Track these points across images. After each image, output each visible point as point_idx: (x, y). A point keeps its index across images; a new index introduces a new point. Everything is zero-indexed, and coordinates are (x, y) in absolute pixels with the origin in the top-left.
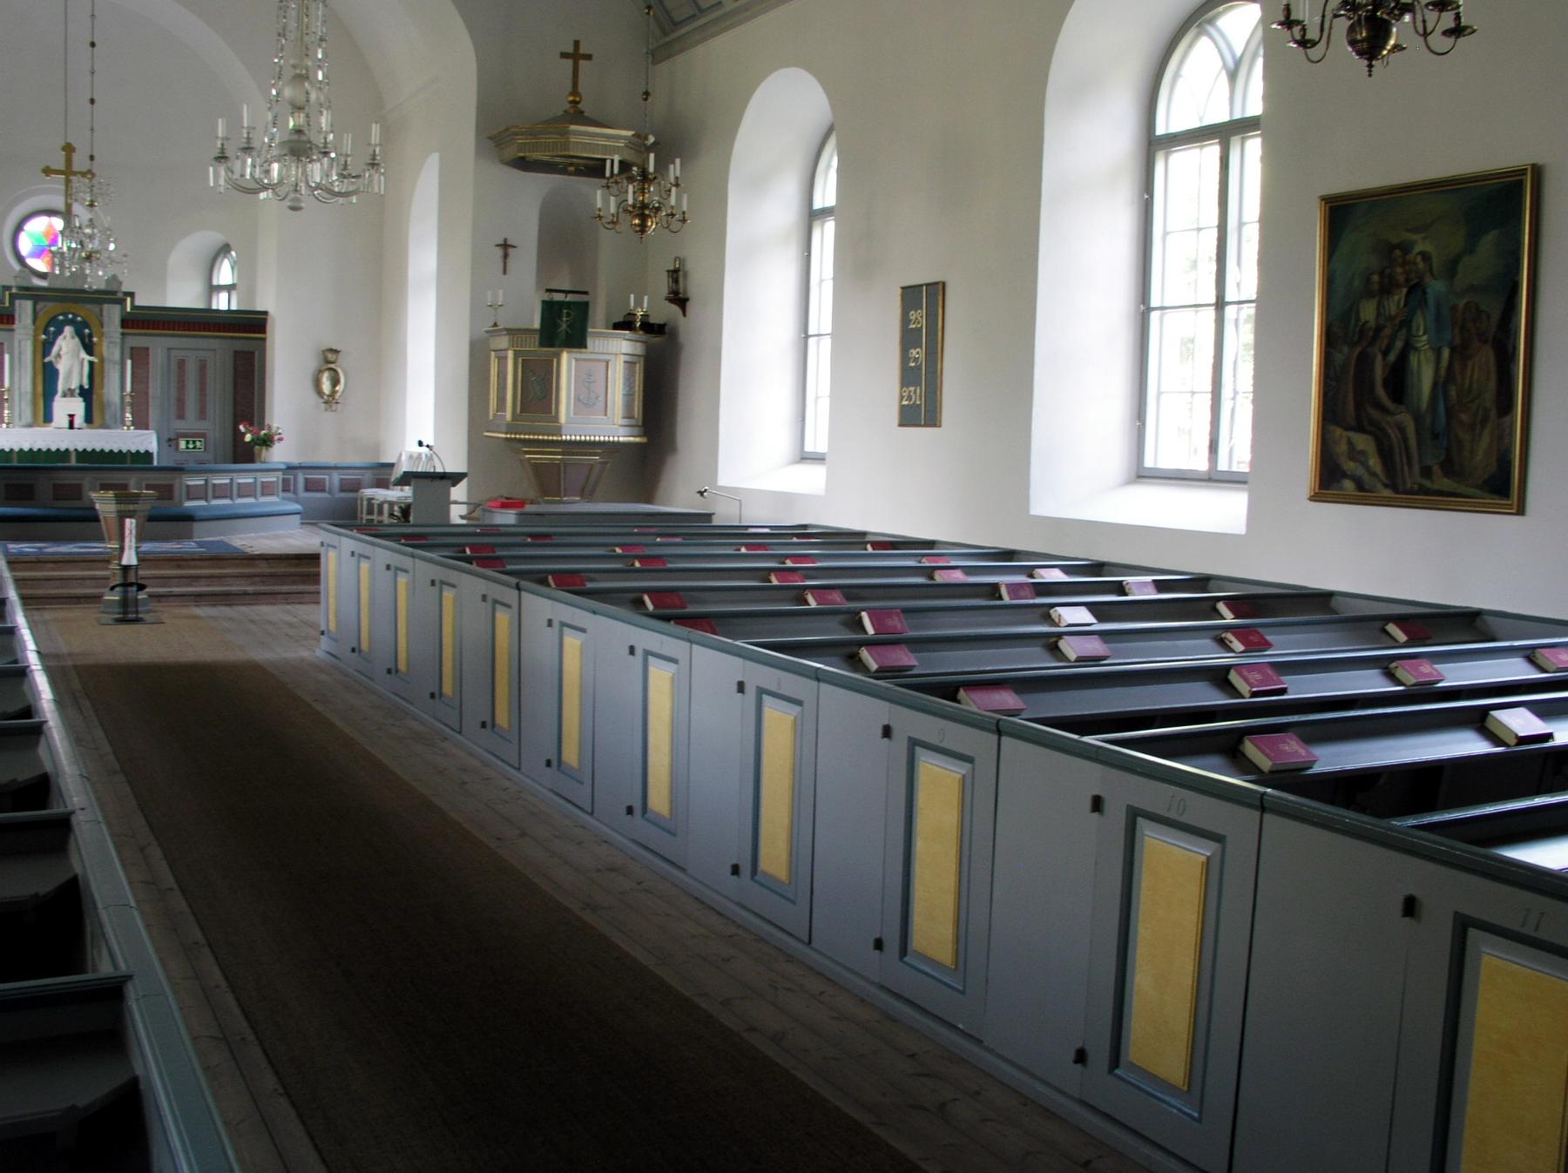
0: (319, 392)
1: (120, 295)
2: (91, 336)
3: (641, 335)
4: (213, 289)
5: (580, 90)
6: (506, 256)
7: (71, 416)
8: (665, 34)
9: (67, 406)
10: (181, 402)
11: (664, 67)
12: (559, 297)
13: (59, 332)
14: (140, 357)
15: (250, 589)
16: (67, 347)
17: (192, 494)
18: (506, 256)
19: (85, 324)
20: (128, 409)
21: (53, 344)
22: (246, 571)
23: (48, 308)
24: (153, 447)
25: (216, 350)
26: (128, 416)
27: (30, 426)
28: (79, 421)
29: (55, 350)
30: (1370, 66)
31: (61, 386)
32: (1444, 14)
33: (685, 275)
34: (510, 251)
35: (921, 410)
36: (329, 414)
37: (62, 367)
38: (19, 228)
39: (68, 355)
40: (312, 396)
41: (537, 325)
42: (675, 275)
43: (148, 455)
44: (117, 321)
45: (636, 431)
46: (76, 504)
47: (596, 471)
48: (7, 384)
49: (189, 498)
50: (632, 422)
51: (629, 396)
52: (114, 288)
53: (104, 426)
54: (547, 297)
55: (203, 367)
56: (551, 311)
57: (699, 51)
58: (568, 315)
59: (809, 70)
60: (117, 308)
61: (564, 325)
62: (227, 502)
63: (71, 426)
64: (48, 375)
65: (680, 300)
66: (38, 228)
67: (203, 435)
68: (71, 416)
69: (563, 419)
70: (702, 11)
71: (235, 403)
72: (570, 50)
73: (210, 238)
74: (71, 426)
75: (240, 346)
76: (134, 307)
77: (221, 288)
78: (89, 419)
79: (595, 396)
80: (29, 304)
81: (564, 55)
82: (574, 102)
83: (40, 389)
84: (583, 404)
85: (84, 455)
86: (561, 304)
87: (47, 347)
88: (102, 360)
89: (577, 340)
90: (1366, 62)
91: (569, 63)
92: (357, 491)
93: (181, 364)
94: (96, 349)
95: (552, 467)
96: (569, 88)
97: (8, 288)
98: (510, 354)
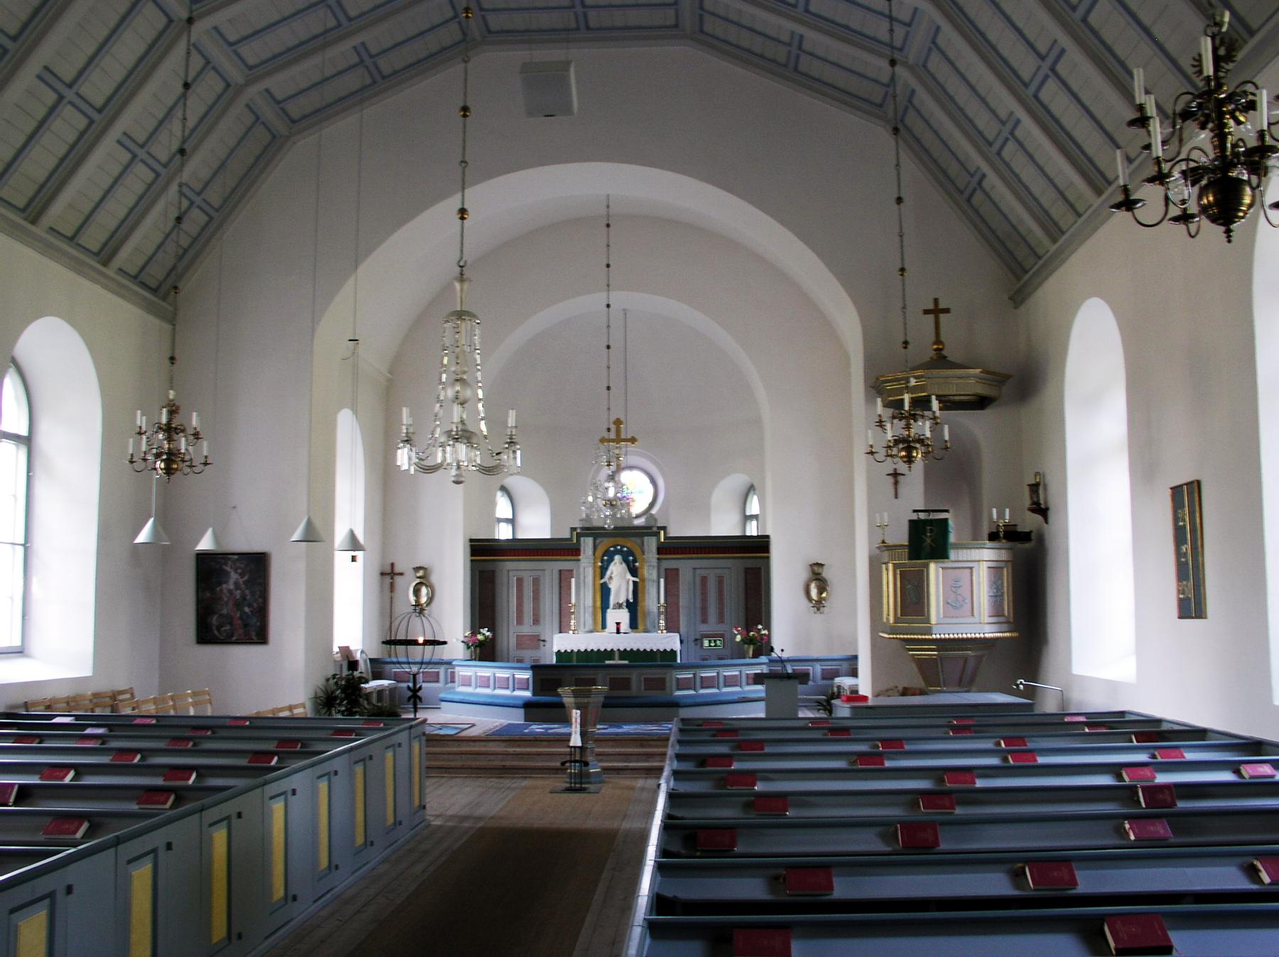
1: (655, 529)
3: (1004, 543)
4: (747, 518)
5: (943, 338)
6: (896, 483)
7: (618, 624)
10: (704, 611)
11: (1022, 309)
12: (922, 516)
13: (611, 560)
14: (671, 577)
16: (617, 569)
17: (682, 685)
18: (896, 483)
19: (630, 553)
20: (662, 617)
21: (607, 569)
23: (605, 543)
24: (677, 646)
25: (730, 568)
26: (662, 622)
27: (591, 632)
28: (625, 627)
29: (608, 573)
30: (1228, 232)
31: (612, 600)
33: (1045, 489)
35: (1192, 607)
36: (818, 616)
37: (613, 586)
38: (653, 482)
39: (619, 579)
42: (1034, 488)
43: (673, 652)
44: (654, 549)
47: (971, 664)
48: (573, 601)
49: (678, 689)
50: (1002, 619)
51: (997, 598)
52: (652, 523)
53: (646, 631)
54: (914, 516)
55: (720, 581)
56: (916, 527)
57: (1040, 293)
58: (931, 531)
59: (1107, 302)
60: (654, 539)
61: (927, 540)
62: (737, 689)
63: (618, 632)
64: (605, 591)
65: (1041, 510)
67: (722, 636)
68: (618, 624)
69: (933, 620)
71: (747, 609)
72: (931, 306)
73: (736, 481)
74: (618, 632)
75: (750, 564)
76: (666, 538)
78: (634, 625)
79: (966, 596)
80: (590, 541)
81: (926, 312)
83: (599, 604)
84: (952, 605)
85: (624, 654)
87: (603, 570)
88: (643, 580)
89: (940, 551)
90: (1223, 229)
91: (931, 317)
92: (832, 679)
93: (704, 580)
94: (640, 571)
95: (954, 660)
96: (933, 339)
98: (890, 566)
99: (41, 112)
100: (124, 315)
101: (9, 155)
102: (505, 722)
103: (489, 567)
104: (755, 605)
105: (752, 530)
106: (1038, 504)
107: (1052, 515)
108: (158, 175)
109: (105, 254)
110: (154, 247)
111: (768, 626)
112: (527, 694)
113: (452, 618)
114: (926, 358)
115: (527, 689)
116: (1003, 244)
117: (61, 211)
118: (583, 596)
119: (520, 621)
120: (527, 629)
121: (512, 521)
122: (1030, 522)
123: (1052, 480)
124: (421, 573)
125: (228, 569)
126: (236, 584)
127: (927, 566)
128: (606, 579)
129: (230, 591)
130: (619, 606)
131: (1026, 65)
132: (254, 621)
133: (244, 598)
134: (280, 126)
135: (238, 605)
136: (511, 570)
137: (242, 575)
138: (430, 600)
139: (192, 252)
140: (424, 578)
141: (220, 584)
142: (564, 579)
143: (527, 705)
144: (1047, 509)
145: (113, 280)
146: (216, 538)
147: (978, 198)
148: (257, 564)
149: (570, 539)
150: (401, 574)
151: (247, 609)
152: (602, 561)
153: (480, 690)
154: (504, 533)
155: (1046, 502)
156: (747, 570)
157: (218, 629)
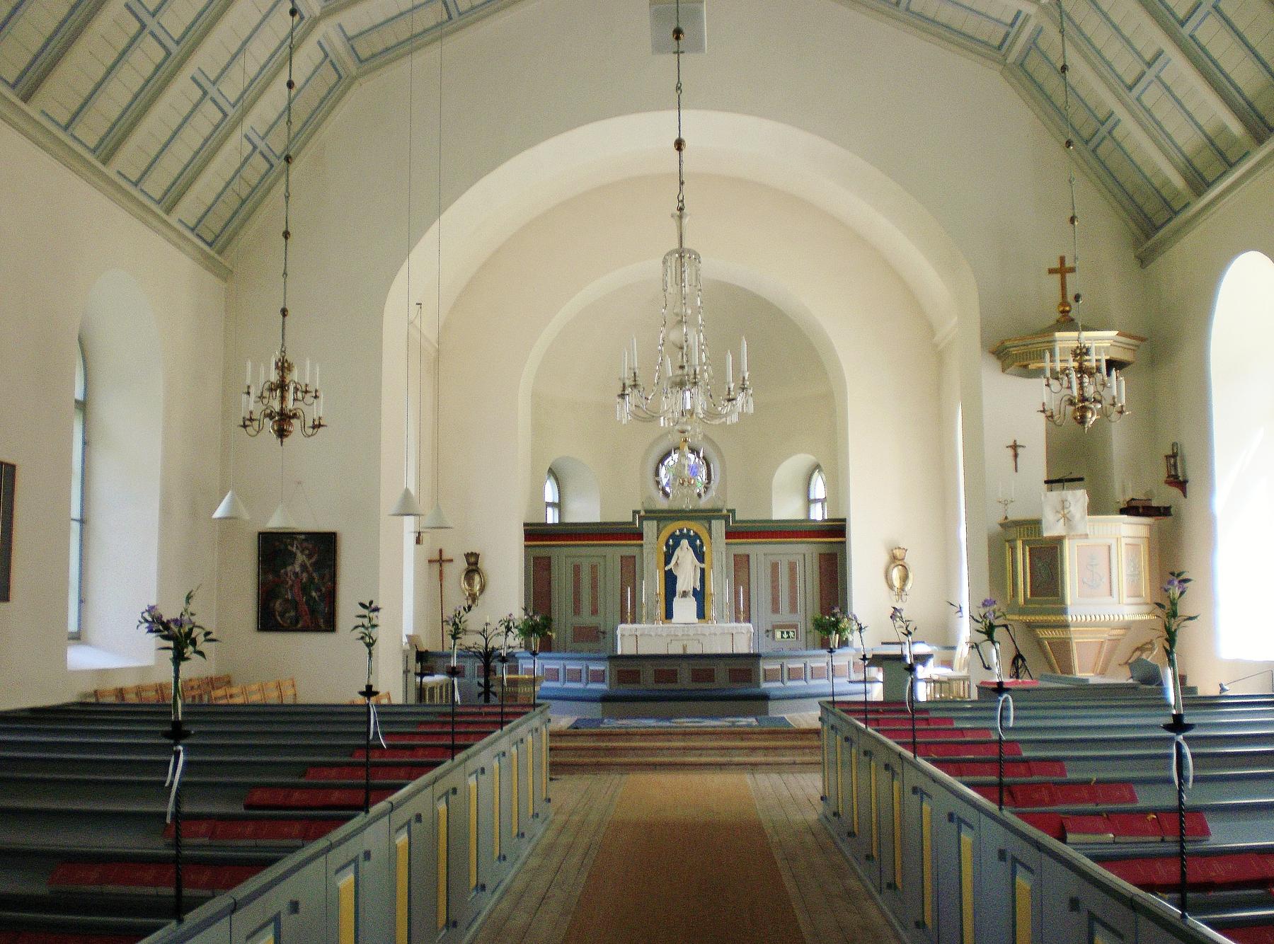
0: (891, 587)
1: (725, 512)
2: (702, 545)
6: (1016, 456)
8: (1148, 237)
9: (685, 609)
13: (677, 544)
15: (798, 759)
16: (685, 557)
17: (770, 676)
18: (1016, 456)
19: (697, 536)
22: (799, 743)
31: (680, 587)
32: (1199, 139)
33: (1183, 460)
34: (1020, 451)
45: (1144, 608)
46: (671, 686)
65: (1180, 483)
70: (1176, 213)
72: (1056, 265)
73: (797, 463)
77: (816, 501)
81: (1051, 271)
82: (1063, 312)
87: (668, 558)
91: (1057, 277)
94: (707, 558)
96: (1060, 300)
97: (638, 512)
98: (1019, 544)
99: (122, 43)
101: (966, 3)
106: (1176, 477)
108: (168, 53)
109: (171, 199)
110: (214, 196)
112: (603, 687)
114: (1052, 322)
115: (603, 681)
116: (1131, 198)
117: (130, 158)
118: (652, 584)
119: (577, 610)
120: (586, 619)
121: (558, 506)
122: (1164, 495)
123: (1187, 450)
124: (472, 560)
125: (294, 549)
126: (303, 566)
128: (671, 566)
129: (296, 574)
130: (685, 594)
132: (322, 607)
133: (311, 579)
134: (353, 68)
135: (305, 589)
136: (563, 557)
137: (310, 556)
138: (482, 589)
140: (473, 566)
141: (285, 566)
143: (605, 699)
144: (1185, 482)
145: (174, 229)
148: (324, 546)
149: (633, 523)
150: (451, 561)
151: (314, 594)
152: (667, 545)
154: (552, 517)
155: (1184, 475)
157: (282, 616)
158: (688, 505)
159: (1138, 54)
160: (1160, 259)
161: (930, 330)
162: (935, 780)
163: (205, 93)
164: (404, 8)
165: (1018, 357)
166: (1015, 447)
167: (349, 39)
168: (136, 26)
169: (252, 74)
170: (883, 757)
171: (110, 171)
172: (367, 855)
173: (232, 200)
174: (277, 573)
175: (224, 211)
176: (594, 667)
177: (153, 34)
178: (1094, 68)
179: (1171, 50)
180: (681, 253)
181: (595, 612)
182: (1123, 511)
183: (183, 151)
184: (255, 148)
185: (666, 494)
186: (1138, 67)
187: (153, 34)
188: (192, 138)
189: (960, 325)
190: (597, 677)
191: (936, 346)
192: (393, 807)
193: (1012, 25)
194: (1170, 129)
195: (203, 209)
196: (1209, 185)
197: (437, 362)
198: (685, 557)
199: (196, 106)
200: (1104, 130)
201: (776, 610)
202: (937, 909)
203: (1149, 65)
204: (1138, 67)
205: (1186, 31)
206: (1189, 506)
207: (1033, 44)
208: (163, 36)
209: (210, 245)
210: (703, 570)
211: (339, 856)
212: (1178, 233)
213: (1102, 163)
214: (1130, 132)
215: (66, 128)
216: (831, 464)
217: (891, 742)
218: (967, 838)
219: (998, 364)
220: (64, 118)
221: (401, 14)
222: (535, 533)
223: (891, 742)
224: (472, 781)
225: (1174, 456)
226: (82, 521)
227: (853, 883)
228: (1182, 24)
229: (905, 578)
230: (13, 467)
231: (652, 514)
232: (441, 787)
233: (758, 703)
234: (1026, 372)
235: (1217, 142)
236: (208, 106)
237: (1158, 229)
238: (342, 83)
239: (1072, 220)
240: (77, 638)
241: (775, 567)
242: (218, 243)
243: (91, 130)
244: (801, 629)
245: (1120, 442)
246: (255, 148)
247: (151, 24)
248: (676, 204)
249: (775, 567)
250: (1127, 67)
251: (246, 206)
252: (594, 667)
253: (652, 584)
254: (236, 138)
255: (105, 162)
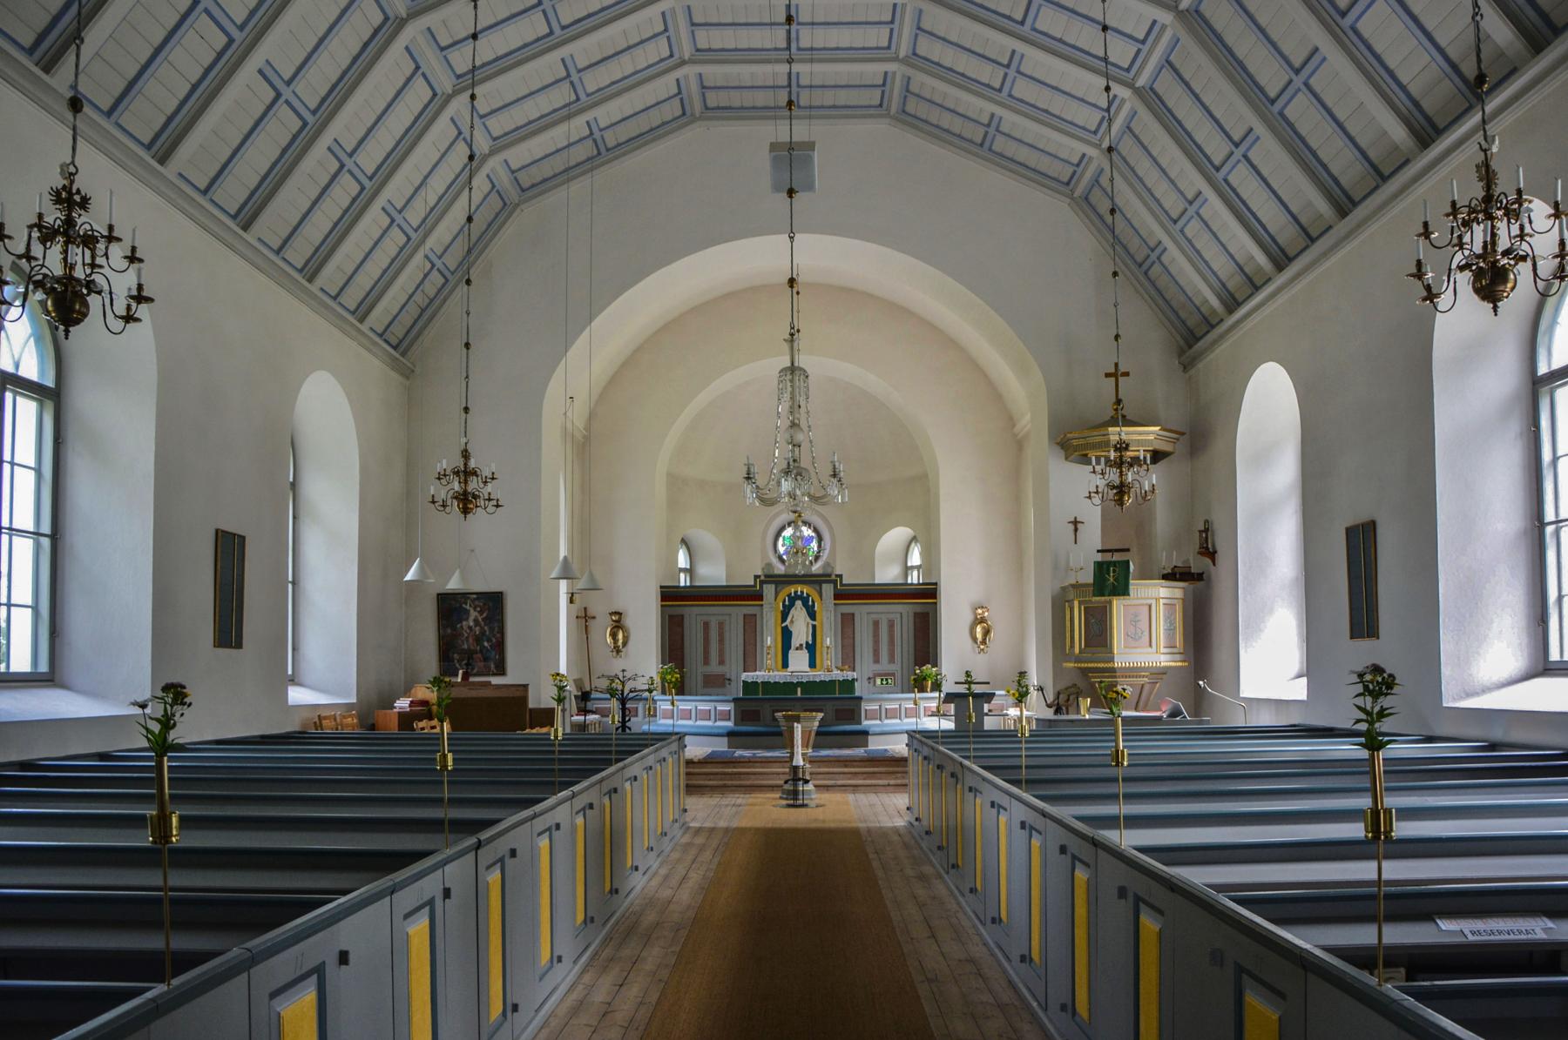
0: (974, 639)
4: (907, 569)
8: (1190, 347)
13: (792, 604)
16: (799, 615)
25: (901, 611)
30: (1495, 309)
31: (795, 642)
40: (970, 641)
41: (1091, 581)
47: (1147, 688)
51: (1170, 631)
54: (1099, 557)
55: (891, 625)
56: (1101, 568)
64: (787, 635)
65: (1209, 552)
66: (896, 535)
70: (1213, 327)
72: (1122, 369)
75: (919, 609)
77: (913, 568)
79: (1145, 631)
81: (1107, 375)
86: (1109, 564)
98: (1076, 603)
99: (325, 180)
100: (373, 366)
102: (710, 750)
103: (679, 611)
104: (925, 645)
105: (914, 578)
107: (1220, 557)
108: (409, 239)
111: (935, 665)
112: (730, 724)
113: (643, 660)
116: (1176, 313)
118: (771, 640)
119: (706, 661)
120: (714, 668)
121: (690, 571)
126: (476, 620)
127: (1110, 603)
130: (800, 648)
131: (1216, 148)
135: (478, 640)
136: (694, 615)
137: (481, 613)
138: (625, 644)
139: (429, 312)
140: (618, 624)
142: (751, 626)
143: (730, 734)
146: (463, 578)
147: (1156, 269)
148: (493, 603)
153: (700, 723)
154: (683, 580)
156: (916, 615)
158: (800, 570)
159: (1182, 193)
160: (1200, 366)
161: (1011, 421)
162: (984, 779)
163: (393, 221)
164: (560, 146)
165: (1076, 448)
166: (1075, 523)
167: (513, 172)
168: (388, 221)
169: (432, 203)
170: (949, 768)
171: (314, 288)
172: (558, 826)
173: (412, 310)
174: (454, 628)
175: (406, 319)
176: (721, 707)
177: (350, 172)
178: (1146, 204)
179: (1209, 193)
180: (793, 369)
181: (722, 662)
182: (1165, 577)
183: (373, 270)
184: (433, 265)
185: (783, 561)
186: (1182, 205)
187: (350, 172)
188: (381, 259)
189: (1032, 416)
190: (725, 716)
191: (1015, 435)
192: (574, 795)
193: (1078, 165)
194: (1207, 256)
195: (390, 318)
196: (1239, 304)
197: (585, 448)
198: (799, 615)
199: (385, 231)
200: (1153, 256)
201: (877, 661)
202: (984, 879)
203: (1191, 203)
204: (1182, 205)
205: (1220, 176)
206: (1220, 573)
207: (1096, 181)
208: (296, 104)
209: (395, 348)
210: (814, 627)
211: (540, 824)
212: (1215, 342)
213: (1153, 283)
214: (1175, 258)
215: (278, 252)
216: (928, 537)
217: (955, 756)
218: (1003, 819)
219: (1062, 453)
220: (276, 245)
221: (558, 151)
222: (670, 595)
223: (955, 756)
224: (627, 785)
225: (1206, 530)
226: (294, 583)
227: (927, 870)
228: (1218, 169)
229: (987, 632)
230: (243, 538)
231: (771, 578)
232: (606, 787)
233: (860, 737)
234: (1085, 460)
235: (1247, 270)
236: (395, 231)
237: (1198, 339)
238: (506, 209)
239: (1117, 337)
240: (293, 681)
241: (876, 624)
242: (404, 347)
243: (299, 253)
244: (898, 675)
245: (1163, 521)
246: (433, 265)
247: (349, 163)
248: (788, 330)
249: (876, 624)
250: (1173, 203)
251: (427, 312)
252: (721, 707)
253: (771, 640)
254: (419, 257)
255: (310, 281)
